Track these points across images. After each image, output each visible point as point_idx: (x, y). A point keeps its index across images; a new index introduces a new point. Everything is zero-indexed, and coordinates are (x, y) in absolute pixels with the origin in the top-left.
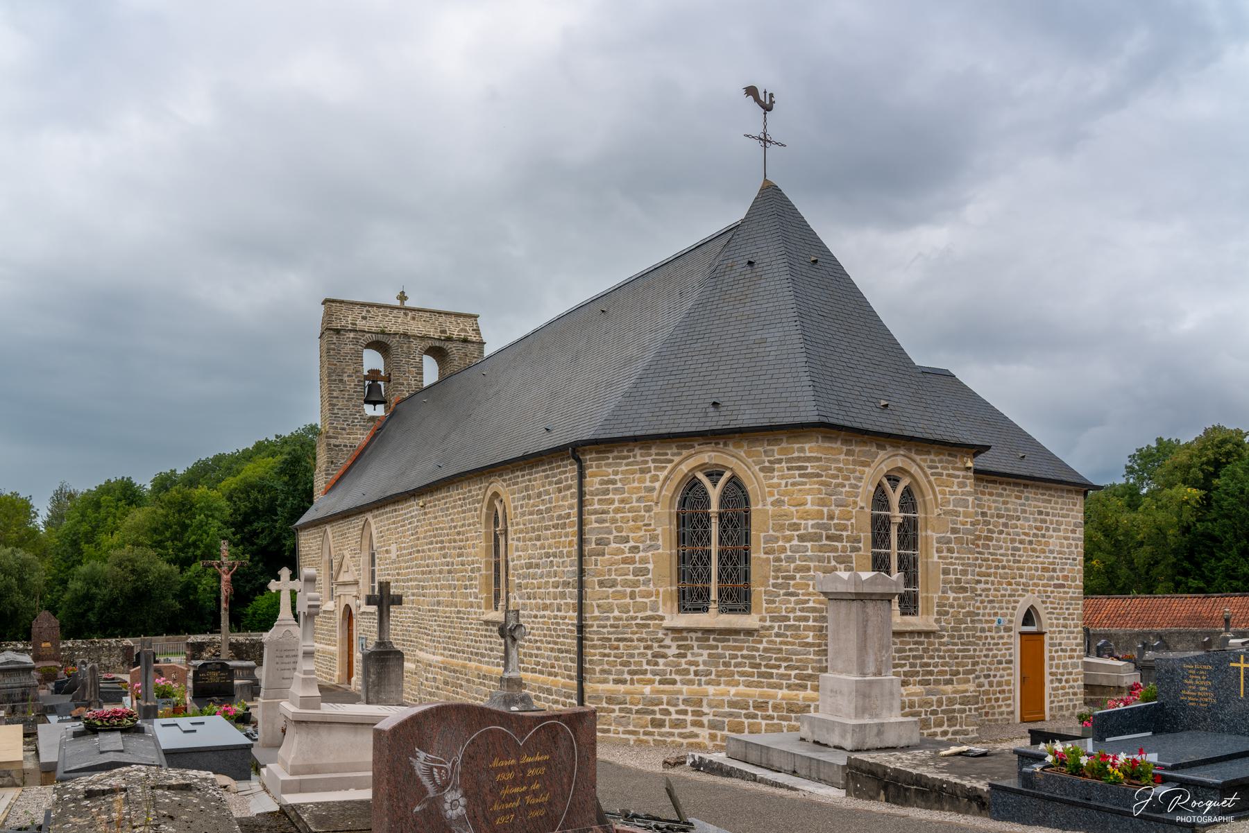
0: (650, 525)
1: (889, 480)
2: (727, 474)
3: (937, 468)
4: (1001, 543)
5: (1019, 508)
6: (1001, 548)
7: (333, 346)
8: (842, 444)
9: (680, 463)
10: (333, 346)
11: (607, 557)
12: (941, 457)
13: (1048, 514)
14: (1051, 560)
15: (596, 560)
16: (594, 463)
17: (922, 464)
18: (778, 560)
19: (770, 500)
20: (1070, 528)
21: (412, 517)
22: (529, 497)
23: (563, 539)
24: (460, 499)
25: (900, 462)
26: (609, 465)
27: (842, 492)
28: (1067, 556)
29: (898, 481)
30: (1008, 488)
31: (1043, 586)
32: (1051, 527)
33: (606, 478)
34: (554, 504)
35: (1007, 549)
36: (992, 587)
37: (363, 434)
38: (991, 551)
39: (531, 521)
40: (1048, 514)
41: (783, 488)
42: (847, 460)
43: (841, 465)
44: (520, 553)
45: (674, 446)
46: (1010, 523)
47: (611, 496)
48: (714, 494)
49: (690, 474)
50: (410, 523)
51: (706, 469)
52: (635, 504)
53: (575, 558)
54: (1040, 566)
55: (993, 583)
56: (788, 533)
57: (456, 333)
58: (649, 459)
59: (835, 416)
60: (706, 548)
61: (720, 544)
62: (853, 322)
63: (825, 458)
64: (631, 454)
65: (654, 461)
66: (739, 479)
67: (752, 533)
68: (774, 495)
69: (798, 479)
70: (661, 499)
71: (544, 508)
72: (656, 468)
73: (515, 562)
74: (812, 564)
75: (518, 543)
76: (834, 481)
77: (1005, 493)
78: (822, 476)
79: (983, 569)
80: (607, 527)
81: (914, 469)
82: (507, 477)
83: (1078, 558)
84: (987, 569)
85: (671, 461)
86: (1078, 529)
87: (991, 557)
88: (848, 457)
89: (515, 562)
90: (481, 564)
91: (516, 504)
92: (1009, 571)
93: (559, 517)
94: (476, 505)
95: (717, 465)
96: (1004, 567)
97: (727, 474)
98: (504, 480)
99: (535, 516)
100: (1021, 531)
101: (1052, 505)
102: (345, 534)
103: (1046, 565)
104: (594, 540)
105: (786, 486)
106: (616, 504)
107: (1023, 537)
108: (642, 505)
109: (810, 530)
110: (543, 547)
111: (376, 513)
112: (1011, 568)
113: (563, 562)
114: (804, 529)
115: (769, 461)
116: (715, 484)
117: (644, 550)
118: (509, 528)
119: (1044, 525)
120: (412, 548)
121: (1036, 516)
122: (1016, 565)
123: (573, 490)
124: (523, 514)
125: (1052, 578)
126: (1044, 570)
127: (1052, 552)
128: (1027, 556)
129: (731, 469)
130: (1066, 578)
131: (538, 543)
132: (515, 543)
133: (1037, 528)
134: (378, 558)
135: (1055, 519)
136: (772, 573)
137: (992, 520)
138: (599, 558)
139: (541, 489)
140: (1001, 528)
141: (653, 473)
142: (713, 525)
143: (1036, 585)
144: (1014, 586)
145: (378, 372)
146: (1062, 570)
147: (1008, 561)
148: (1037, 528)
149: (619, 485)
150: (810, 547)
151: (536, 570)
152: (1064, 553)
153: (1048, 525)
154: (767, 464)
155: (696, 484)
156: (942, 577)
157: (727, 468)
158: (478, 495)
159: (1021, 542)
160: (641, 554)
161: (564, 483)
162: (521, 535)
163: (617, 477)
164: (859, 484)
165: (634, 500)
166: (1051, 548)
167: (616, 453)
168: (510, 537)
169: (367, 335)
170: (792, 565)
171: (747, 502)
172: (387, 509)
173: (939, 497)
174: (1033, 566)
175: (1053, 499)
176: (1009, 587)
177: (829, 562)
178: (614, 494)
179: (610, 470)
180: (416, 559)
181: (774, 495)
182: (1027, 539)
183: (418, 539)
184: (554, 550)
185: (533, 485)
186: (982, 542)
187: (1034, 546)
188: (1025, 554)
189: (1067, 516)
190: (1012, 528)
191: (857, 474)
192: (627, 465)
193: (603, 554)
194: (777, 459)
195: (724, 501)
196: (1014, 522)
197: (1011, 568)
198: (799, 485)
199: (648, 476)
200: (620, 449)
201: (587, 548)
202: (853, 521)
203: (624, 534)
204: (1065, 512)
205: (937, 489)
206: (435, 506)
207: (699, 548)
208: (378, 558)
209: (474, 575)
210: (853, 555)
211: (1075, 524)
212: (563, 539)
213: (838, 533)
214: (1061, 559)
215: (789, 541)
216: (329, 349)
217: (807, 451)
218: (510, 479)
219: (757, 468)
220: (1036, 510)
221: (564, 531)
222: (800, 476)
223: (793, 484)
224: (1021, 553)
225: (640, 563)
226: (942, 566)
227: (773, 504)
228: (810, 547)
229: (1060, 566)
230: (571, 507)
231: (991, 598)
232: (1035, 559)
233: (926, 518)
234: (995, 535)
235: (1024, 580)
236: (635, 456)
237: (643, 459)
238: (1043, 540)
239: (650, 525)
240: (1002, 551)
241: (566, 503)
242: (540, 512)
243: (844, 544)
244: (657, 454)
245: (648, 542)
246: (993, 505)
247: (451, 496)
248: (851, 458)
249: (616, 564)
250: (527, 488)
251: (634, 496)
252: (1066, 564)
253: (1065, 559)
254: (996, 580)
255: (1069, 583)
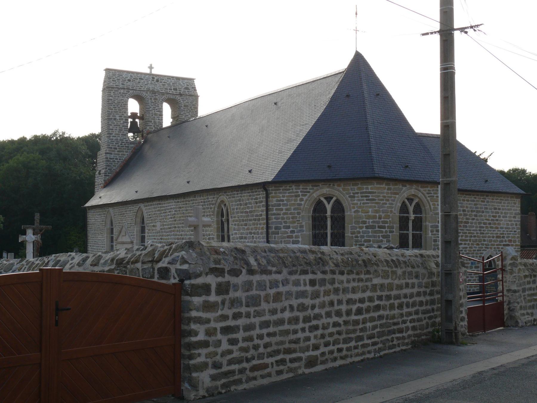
0: (300, 221)
1: (408, 200)
2: (334, 199)
3: (431, 193)
4: (473, 225)
5: (484, 207)
6: (473, 227)
7: (111, 98)
8: (385, 185)
9: (313, 193)
10: (111, 98)
11: (280, 235)
12: (434, 188)
13: (499, 209)
14: (502, 232)
15: (275, 237)
16: (273, 192)
17: (424, 192)
18: (357, 237)
19: (353, 210)
20: (512, 216)
21: (171, 208)
22: (241, 205)
23: (259, 226)
24: (202, 202)
25: (413, 191)
26: (280, 193)
27: (385, 207)
28: (511, 230)
29: (413, 200)
30: (477, 197)
31: (497, 245)
32: (502, 215)
33: (279, 199)
34: (254, 209)
35: (477, 227)
36: (468, 246)
37: (127, 152)
38: (468, 228)
39: (242, 216)
40: (499, 209)
41: (359, 205)
42: (388, 192)
43: (385, 195)
44: (236, 232)
45: (310, 185)
46: (478, 214)
47: (281, 207)
48: (329, 207)
49: (318, 198)
50: (170, 212)
51: (325, 196)
52: (292, 211)
53: (265, 235)
54: (495, 235)
55: (469, 244)
56: (361, 225)
57: (182, 90)
58: (299, 191)
59: (382, 173)
60: (325, 231)
61: (331, 230)
62: (395, 124)
63: (377, 192)
64: (291, 188)
65: (301, 192)
66: (339, 200)
67: (346, 225)
68: (355, 208)
69: (365, 201)
70: (304, 209)
71: (248, 210)
72: (302, 195)
73: (234, 236)
74: (371, 239)
75: (235, 226)
76: (382, 202)
77: (475, 200)
78: (376, 200)
79: (464, 238)
80: (280, 221)
81: (420, 195)
82: (229, 194)
83: (517, 231)
84: (465, 237)
85: (309, 192)
86: (517, 216)
87: (468, 232)
88: (388, 191)
89: (234, 236)
90: (214, 236)
91: (234, 207)
92: (478, 239)
93: (257, 216)
94: (211, 206)
95: (330, 194)
96: (475, 236)
97: (334, 199)
98: (227, 195)
99: (244, 214)
100: (484, 218)
101: (502, 204)
102: (124, 214)
103: (499, 235)
104: (274, 227)
105: (360, 204)
106: (284, 211)
107: (485, 221)
108: (296, 211)
109: (371, 224)
110: (248, 229)
111: (146, 204)
112: (478, 237)
113: (259, 237)
114: (368, 223)
115: (353, 193)
116: (329, 203)
117: (297, 232)
118: (230, 219)
119: (497, 215)
120: (171, 225)
121: (493, 210)
122: (481, 235)
123: (263, 203)
124: (237, 213)
125: (502, 241)
126: (497, 237)
127: (502, 228)
128: (487, 231)
129: (336, 196)
130: (510, 241)
131: (246, 227)
132: (234, 226)
133: (493, 216)
134: (147, 229)
135: (503, 211)
136: (354, 243)
137: (468, 213)
138: (276, 235)
139: (247, 201)
140: (473, 217)
141: (301, 197)
142: (328, 221)
143: (493, 245)
144: (480, 246)
145: (137, 114)
146: (508, 237)
147: (477, 233)
148: (493, 216)
149: (285, 202)
150: (370, 231)
151: (245, 240)
152: (509, 228)
153: (500, 214)
154: (352, 194)
155: (320, 202)
156: (433, 243)
157: (334, 196)
158: (212, 201)
159: (485, 224)
160: (296, 234)
161: (259, 200)
162: (237, 223)
163: (285, 199)
164: (394, 203)
165: (292, 209)
166: (502, 226)
167: (284, 188)
168: (230, 223)
169: (131, 92)
170: (363, 239)
171: (343, 211)
172: (155, 203)
173: (432, 207)
174: (491, 235)
175: (503, 201)
176: (477, 246)
177: (379, 238)
178: (283, 206)
179: (281, 195)
180: (173, 231)
181: (355, 208)
182: (488, 222)
183: (175, 221)
184: (254, 231)
185: (243, 199)
186: (463, 224)
187: (492, 225)
188: (487, 230)
189: (511, 209)
190: (479, 217)
191: (393, 198)
192: (289, 193)
193: (278, 234)
194: (357, 192)
195: (333, 211)
196: (481, 214)
197: (478, 237)
198: (366, 204)
199: (298, 198)
200: (285, 186)
201: (270, 231)
202: (391, 219)
203: (288, 225)
204: (509, 208)
205: (431, 203)
206: (186, 204)
207: (322, 231)
208: (147, 229)
209: (210, 241)
210: (390, 234)
211: (515, 214)
212: (259, 226)
213: (383, 225)
214: (508, 231)
215: (362, 229)
216: (109, 99)
217: (369, 189)
218: (231, 195)
219: (347, 196)
220: (493, 207)
221: (259, 222)
222: (367, 200)
223: (363, 204)
224: (485, 229)
225: (295, 238)
226: (433, 238)
227: (355, 212)
228: (370, 231)
229: (507, 235)
230: (262, 211)
231: (468, 252)
232: (492, 232)
233: (426, 217)
234: (470, 221)
235: (486, 243)
236: (292, 189)
237: (296, 190)
238: (497, 222)
239: (300, 221)
240: (474, 229)
241: (260, 209)
242: (246, 212)
243: (386, 230)
244: (302, 189)
245: (299, 229)
246: (469, 206)
247: (196, 200)
248: (390, 191)
249: (284, 238)
250: (239, 200)
251: (292, 208)
252: (510, 234)
253: (510, 231)
254: (470, 243)
255: (512, 243)
